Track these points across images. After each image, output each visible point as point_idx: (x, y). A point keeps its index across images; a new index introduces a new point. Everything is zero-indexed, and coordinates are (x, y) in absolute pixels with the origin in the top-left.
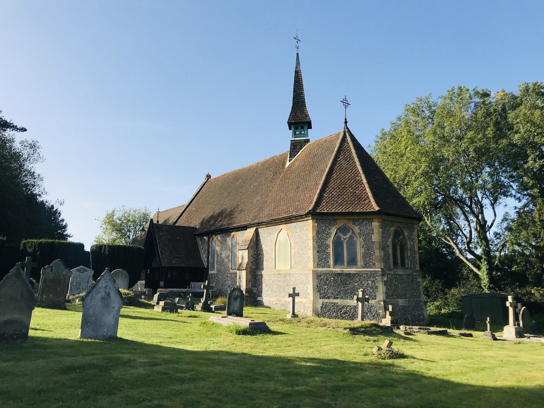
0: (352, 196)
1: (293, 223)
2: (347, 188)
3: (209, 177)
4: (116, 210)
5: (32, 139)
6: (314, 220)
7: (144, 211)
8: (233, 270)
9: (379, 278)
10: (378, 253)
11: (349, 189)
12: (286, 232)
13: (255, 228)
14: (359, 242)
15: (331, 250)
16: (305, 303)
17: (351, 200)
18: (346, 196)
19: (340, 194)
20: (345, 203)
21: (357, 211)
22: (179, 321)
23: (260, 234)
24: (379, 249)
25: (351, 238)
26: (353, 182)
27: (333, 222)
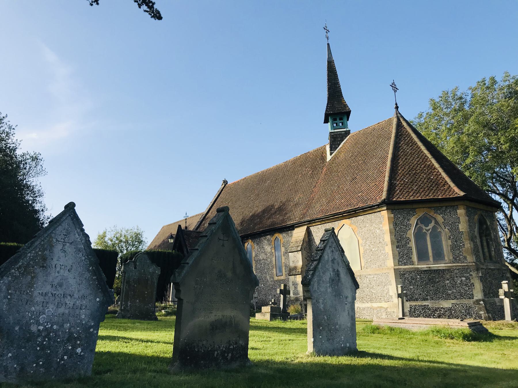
0: (427, 181)
1: (359, 217)
2: (418, 173)
3: (225, 182)
4: (108, 231)
5: (34, 152)
6: (389, 211)
7: (136, 231)
8: (279, 277)
9: (475, 273)
10: (468, 245)
11: (422, 175)
12: (350, 228)
13: (305, 227)
14: (445, 233)
15: (413, 244)
16: (388, 307)
17: (427, 187)
18: (421, 182)
19: (413, 181)
20: (422, 190)
21: (440, 197)
22: (159, 342)
23: (313, 233)
24: (469, 240)
25: (434, 228)
26: (424, 167)
27: (411, 212)
